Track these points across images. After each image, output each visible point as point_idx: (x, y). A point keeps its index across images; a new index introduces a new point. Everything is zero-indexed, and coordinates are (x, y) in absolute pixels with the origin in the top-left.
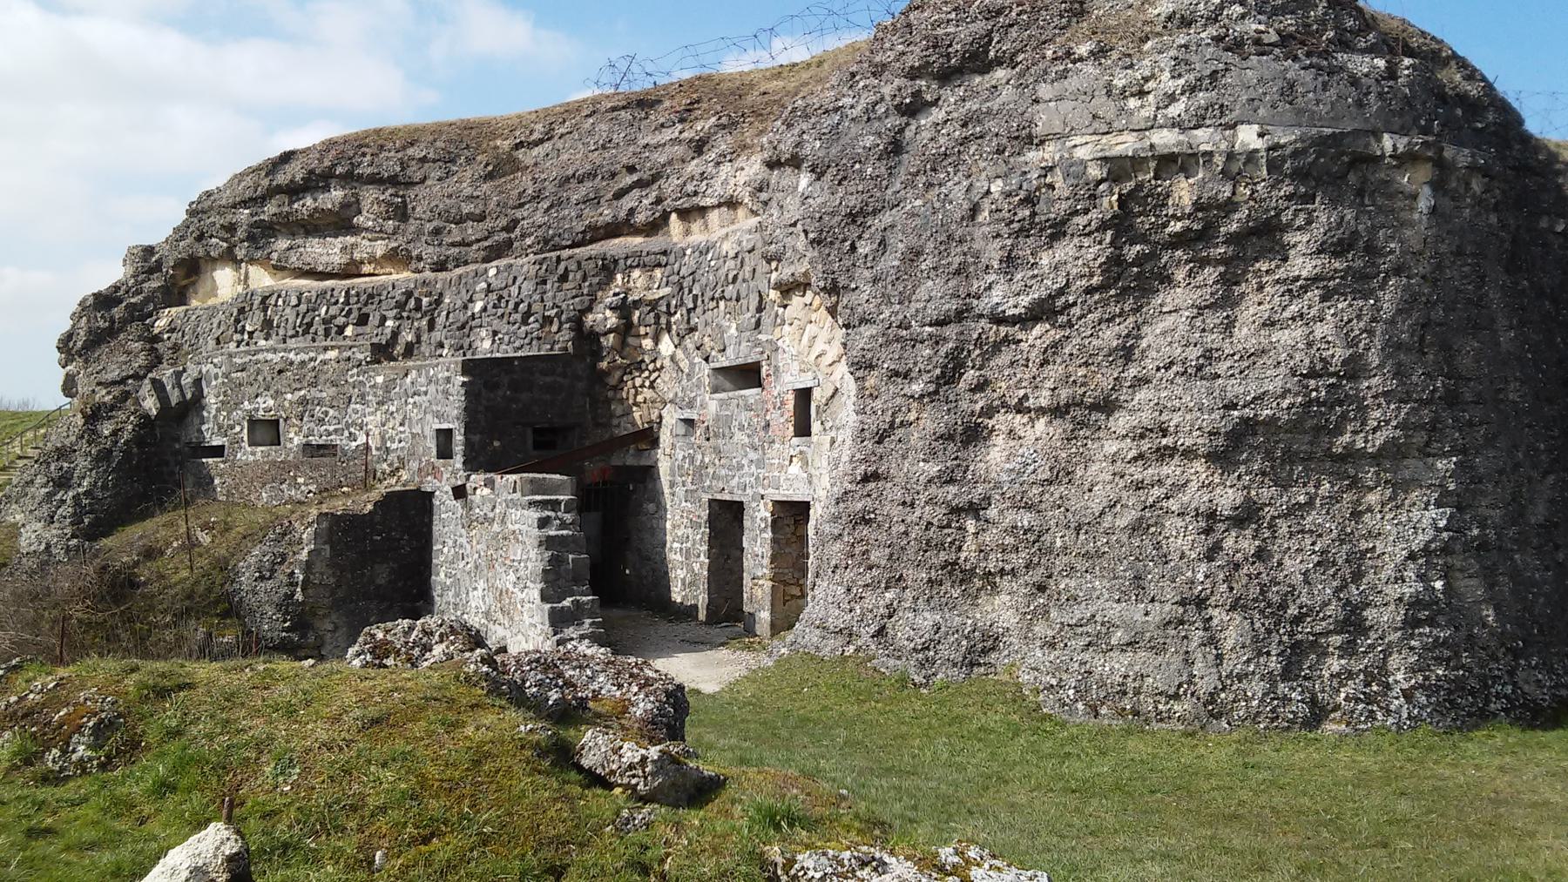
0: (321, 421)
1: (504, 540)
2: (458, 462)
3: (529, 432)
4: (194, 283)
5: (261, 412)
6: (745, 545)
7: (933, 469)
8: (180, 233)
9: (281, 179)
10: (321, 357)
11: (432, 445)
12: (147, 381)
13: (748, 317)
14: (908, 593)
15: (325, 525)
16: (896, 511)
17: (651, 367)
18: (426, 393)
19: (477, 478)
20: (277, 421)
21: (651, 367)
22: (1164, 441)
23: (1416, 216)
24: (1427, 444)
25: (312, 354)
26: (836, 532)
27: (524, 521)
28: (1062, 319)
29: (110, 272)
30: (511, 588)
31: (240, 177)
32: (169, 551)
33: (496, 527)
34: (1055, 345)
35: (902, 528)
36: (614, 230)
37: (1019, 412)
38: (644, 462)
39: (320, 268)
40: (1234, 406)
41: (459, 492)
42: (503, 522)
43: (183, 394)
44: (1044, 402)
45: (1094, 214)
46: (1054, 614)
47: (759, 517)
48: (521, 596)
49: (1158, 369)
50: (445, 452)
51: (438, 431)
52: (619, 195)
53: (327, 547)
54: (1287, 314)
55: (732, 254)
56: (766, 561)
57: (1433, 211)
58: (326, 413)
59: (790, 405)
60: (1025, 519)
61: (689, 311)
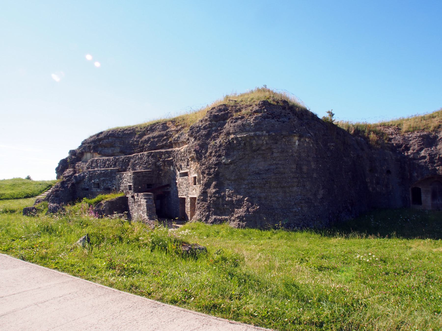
0: (107, 184)
1: (140, 205)
2: (132, 191)
3: (146, 185)
4: (82, 157)
5: (96, 182)
6: (186, 205)
7: (214, 190)
8: (80, 147)
9: (100, 137)
10: (107, 171)
11: (128, 188)
12: (73, 176)
13: (186, 163)
14: (211, 213)
15: (107, 203)
16: (209, 198)
17: (169, 173)
18: (127, 178)
19: (136, 194)
20: (99, 184)
21: (169, 173)
22: (252, 185)
23: (295, 146)
24: (298, 185)
25: (106, 171)
26: (199, 202)
27: (143, 202)
28: (235, 164)
29: (65, 155)
30: (142, 214)
31: (91, 137)
32: (201, 176)
33: (139, 203)
34: (235, 169)
35: (209, 201)
36: (162, 147)
37: (229, 180)
38: (168, 190)
39: (107, 154)
40: (264, 179)
41: (133, 197)
42: (140, 202)
43: (164, 222)
44: (233, 179)
45: (240, 146)
46: (234, 215)
47: (188, 200)
48: (143, 215)
49: (251, 172)
50: (130, 189)
51: (129, 185)
52: (164, 140)
53: (108, 207)
54: (273, 163)
55: (183, 152)
56: (189, 209)
57: (299, 145)
58: (108, 182)
59: (193, 180)
60: (230, 199)
61: (176, 162)
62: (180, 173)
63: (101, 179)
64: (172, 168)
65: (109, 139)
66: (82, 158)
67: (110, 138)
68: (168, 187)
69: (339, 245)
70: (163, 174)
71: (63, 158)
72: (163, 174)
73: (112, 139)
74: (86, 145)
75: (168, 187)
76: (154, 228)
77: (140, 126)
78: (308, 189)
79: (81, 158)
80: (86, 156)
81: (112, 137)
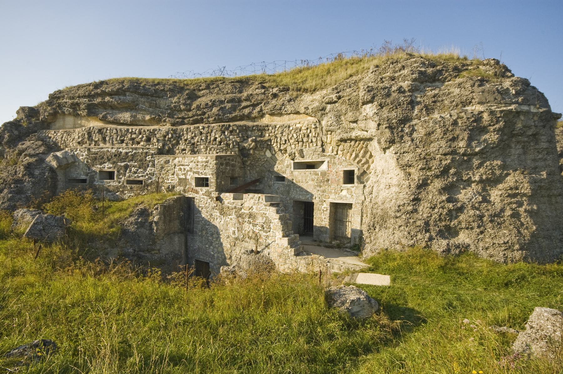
17: (263, 160)
28: (484, 156)
62: (294, 163)
63: (119, 164)
64: (268, 154)
65: (125, 95)
66: (53, 124)
67: (128, 94)
68: (258, 184)
69: (433, 234)
70: (249, 162)
71: (8, 121)
72: (249, 162)
73: (132, 96)
74: (233, 115)
75: (258, 184)
76: (73, 306)
77: (147, 81)
78: (86, 195)
79: (50, 123)
80: (64, 121)
81: (132, 92)
